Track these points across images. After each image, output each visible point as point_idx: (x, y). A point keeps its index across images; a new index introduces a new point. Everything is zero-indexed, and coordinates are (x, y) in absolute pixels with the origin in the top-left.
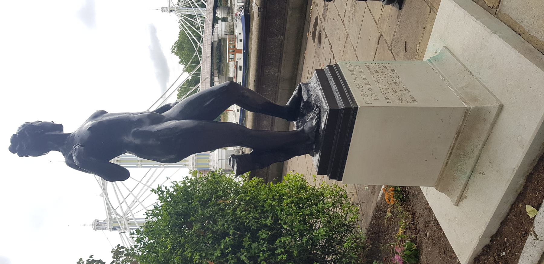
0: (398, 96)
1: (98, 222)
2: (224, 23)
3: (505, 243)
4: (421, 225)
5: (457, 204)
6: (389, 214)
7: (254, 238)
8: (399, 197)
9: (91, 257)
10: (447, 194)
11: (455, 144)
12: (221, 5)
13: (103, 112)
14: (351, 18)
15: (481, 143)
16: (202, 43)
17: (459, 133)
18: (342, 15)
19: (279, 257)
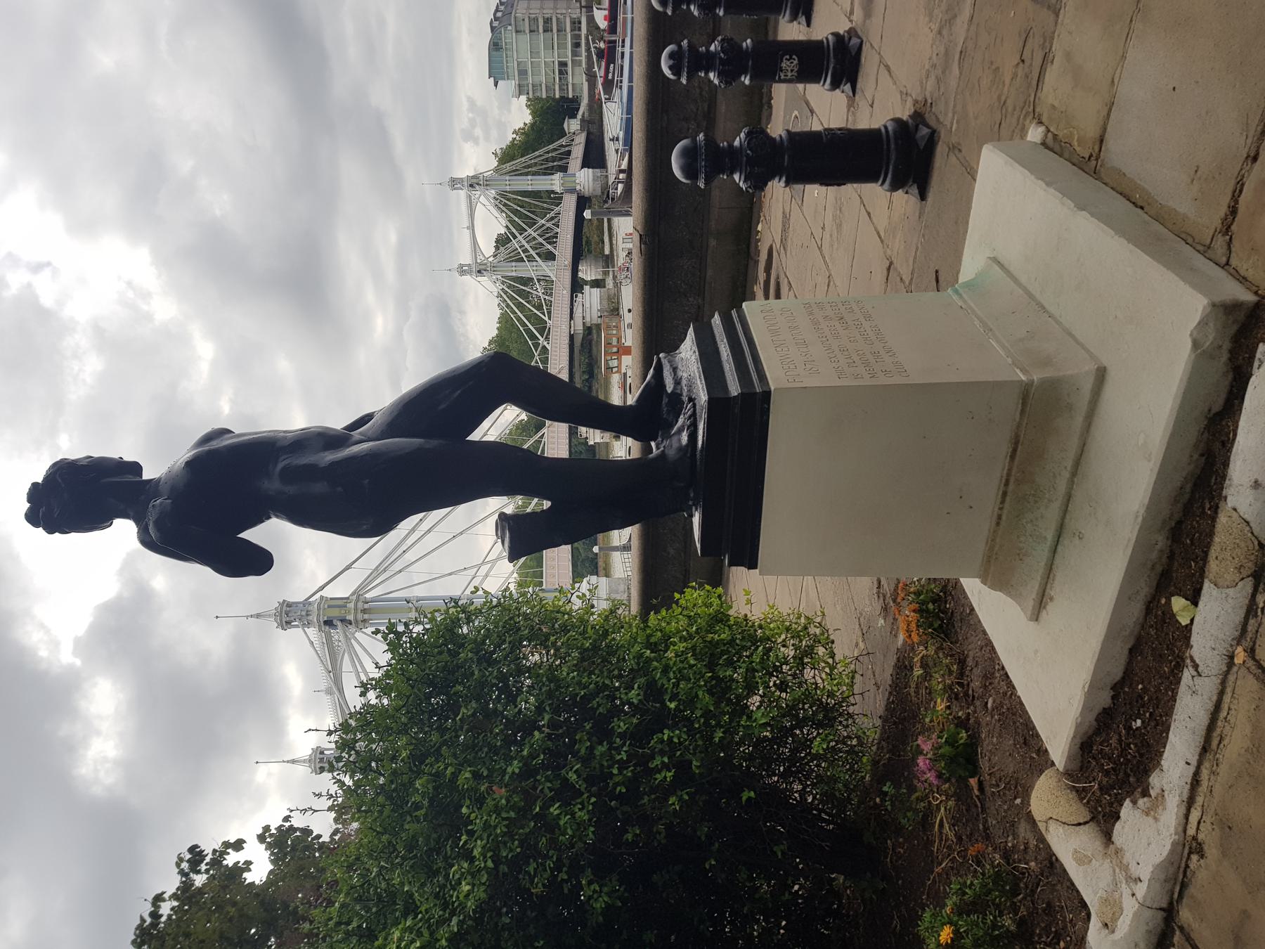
1: (322, 753)
2: (596, 291)
4: (976, 684)
5: (1036, 617)
6: (918, 672)
7: (603, 732)
9: (286, 819)
10: (1009, 594)
11: (1010, 470)
12: (590, 252)
13: (225, 432)
15: (1069, 464)
16: (547, 339)
19: (658, 776)
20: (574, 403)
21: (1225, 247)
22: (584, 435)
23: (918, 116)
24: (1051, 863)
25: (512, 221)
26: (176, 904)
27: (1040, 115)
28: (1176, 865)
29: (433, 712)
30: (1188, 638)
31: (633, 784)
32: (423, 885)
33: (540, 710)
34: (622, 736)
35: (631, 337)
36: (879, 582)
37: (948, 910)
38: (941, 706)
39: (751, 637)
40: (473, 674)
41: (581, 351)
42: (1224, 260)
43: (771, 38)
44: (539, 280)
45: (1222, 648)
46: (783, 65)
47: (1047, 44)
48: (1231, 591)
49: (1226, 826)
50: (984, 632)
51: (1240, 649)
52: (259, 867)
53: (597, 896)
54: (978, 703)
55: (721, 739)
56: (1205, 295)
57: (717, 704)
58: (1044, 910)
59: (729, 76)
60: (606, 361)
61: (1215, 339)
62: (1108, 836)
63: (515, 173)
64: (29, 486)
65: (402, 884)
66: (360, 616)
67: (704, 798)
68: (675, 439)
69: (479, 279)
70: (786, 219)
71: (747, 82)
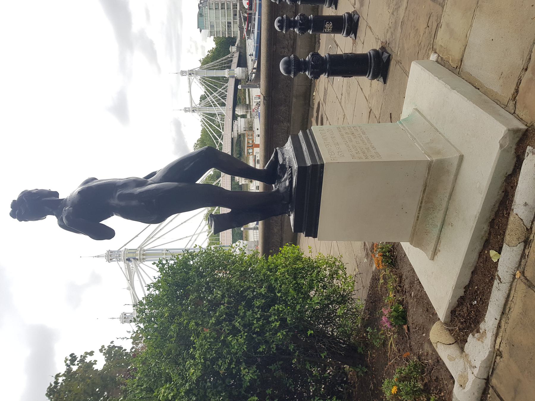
0: (364, 153)
1: (125, 315)
2: (243, 119)
3: (476, 292)
4: (407, 286)
5: (433, 259)
6: (381, 281)
7: (249, 306)
8: (387, 262)
9: (112, 342)
10: (421, 249)
11: (423, 197)
14: (347, 98)
15: (447, 195)
16: (222, 139)
17: (426, 186)
18: (339, 97)
19: (273, 324)
20: (235, 166)
21: (514, 106)
22: (237, 181)
23: (383, 48)
24: (438, 361)
25: (207, 89)
26: (64, 378)
27: (435, 49)
28: (491, 360)
29: (178, 297)
30: (496, 267)
31: (262, 327)
32: (174, 370)
33: (223, 296)
34: (258, 307)
35: (258, 140)
36: (365, 244)
37: (395, 379)
38: (391, 295)
39: (312, 267)
40: (195, 281)
41: (236, 145)
42: (513, 111)
43: (319, 14)
44: (218, 115)
45: (511, 272)
46: (326, 26)
47: (439, 20)
48: (515, 248)
49: (512, 345)
50: (410, 265)
51: (518, 272)
52: (100, 363)
53: (248, 375)
54: (407, 294)
55: (299, 309)
56: (505, 126)
57: (297, 295)
58: (435, 380)
59: (303, 30)
60: (247, 150)
61: (509, 144)
62: (462, 349)
63: (209, 69)
64: (12, 201)
65: (165, 369)
66: (142, 257)
67: (292, 333)
68: (283, 183)
69: (193, 114)
70: (326, 90)
71: (311, 33)
